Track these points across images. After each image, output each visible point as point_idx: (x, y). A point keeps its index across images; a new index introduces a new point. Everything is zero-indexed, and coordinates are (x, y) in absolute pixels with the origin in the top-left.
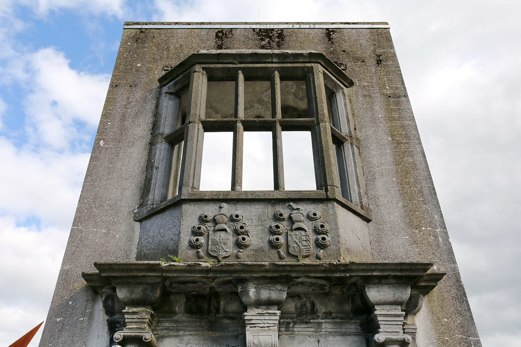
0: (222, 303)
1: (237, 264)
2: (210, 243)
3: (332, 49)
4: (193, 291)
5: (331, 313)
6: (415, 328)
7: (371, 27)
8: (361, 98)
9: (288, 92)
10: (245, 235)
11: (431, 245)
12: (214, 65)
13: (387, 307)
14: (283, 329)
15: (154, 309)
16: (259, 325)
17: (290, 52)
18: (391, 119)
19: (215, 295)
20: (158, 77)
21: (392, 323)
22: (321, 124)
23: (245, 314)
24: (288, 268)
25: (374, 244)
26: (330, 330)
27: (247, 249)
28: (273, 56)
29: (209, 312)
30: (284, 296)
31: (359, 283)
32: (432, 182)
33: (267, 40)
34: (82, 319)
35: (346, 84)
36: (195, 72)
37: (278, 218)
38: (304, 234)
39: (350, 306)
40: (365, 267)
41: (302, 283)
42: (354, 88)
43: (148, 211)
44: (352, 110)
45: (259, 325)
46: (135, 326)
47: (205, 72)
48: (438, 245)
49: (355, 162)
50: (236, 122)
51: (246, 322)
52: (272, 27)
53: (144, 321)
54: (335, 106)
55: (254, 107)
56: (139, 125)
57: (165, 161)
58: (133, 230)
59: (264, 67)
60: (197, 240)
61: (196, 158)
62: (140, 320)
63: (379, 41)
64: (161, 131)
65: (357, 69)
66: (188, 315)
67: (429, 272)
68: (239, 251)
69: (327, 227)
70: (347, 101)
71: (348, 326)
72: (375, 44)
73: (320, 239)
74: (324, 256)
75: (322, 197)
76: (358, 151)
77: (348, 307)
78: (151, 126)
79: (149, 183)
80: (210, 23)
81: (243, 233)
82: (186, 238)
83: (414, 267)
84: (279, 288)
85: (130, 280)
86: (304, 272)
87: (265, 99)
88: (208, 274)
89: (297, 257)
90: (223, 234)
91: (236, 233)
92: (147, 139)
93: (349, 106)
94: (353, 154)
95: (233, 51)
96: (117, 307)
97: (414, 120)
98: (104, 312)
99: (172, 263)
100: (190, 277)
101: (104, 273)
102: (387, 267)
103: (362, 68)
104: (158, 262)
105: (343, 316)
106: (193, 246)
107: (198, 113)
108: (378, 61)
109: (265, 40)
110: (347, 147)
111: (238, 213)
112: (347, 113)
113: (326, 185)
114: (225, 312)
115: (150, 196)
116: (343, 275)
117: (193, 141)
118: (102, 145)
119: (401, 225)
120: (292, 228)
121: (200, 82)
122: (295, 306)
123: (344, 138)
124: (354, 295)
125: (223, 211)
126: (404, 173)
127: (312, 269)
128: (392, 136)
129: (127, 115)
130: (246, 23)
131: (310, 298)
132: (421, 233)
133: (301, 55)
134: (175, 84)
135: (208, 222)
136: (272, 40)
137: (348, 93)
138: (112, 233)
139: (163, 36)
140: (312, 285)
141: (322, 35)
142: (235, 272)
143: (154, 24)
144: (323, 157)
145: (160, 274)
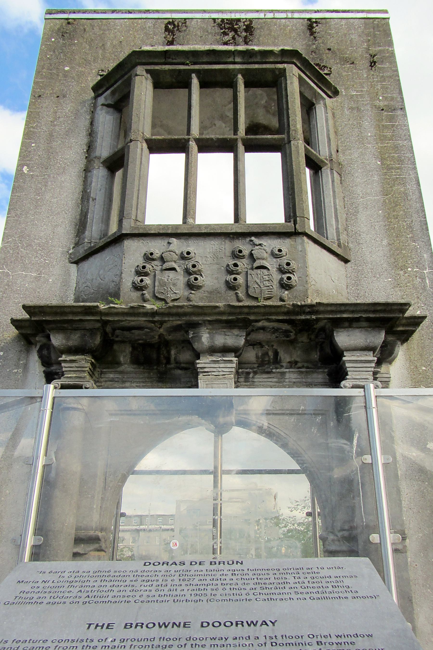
0: (173, 352)
1: (187, 306)
2: (157, 284)
3: (314, 46)
4: (139, 340)
5: (296, 362)
6: (388, 376)
7: (365, 17)
8: (347, 112)
9: (257, 104)
10: (198, 274)
11: (416, 289)
12: (160, 66)
13: (358, 353)
14: (242, 380)
15: (94, 357)
16: (213, 373)
17: (256, 48)
18: (382, 138)
19: (164, 344)
20: (91, 85)
21: (361, 369)
22: (292, 142)
23: (197, 361)
24: (246, 310)
25: (351, 287)
26: (294, 380)
27: (200, 291)
28: (236, 53)
29: (158, 363)
30: (242, 342)
31: (327, 326)
32: (425, 215)
33: (231, 34)
34: (16, 371)
35: (329, 93)
36: (137, 75)
37: (237, 255)
38: (267, 273)
39: (318, 353)
40: (333, 308)
41: (263, 328)
42: (338, 99)
43: (85, 250)
44: (335, 126)
45: (213, 373)
46: (75, 375)
47: (149, 75)
48: (424, 288)
49: (334, 192)
50: (188, 140)
51: (199, 370)
52: (238, 16)
53: (84, 369)
54: (314, 122)
55: (215, 125)
56: (71, 147)
57: (103, 191)
58: (68, 273)
59: (224, 70)
60: (142, 281)
61: (139, 185)
62: (79, 369)
63: (375, 35)
64: (97, 153)
65: (344, 74)
66: (135, 366)
67: (407, 314)
68: (191, 293)
69: (293, 265)
70: (330, 115)
71: (315, 375)
72: (369, 40)
73: (285, 278)
74: (289, 298)
75: (291, 230)
76: (339, 178)
77: (315, 356)
78: (85, 148)
79: (85, 218)
80: (158, 11)
81: (195, 273)
82: (129, 278)
83: (389, 308)
84: (236, 333)
85: (66, 325)
86: (264, 314)
87: (228, 115)
88: (154, 317)
89: (257, 298)
90: (171, 274)
91: (188, 272)
92: (82, 164)
93: (331, 122)
94: (333, 181)
95: (186, 48)
96: (53, 356)
97: (410, 140)
98: (41, 364)
99: (112, 305)
100: (134, 321)
101: (34, 316)
102: (358, 308)
103: (351, 72)
104: (95, 304)
105: (310, 366)
106: (137, 288)
107: (141, 129)
108: (371, 63)
109: (228, 34)
110: (326, 172)
111: (190, 249)
112: (328, 130)
113: (295, 216)
114: (177, 363)
115: (87, 233)
116: (308, 317)
117: (135, 164)
118: (26, 172)
119: (385, 265)
120: (253, 267)
121: (143, 89)
122: (256, 354)
123: (323, 161)
124: (323, 342)
125: (172, 247)
126: (393, 205)
127: (273, 310)
128: (382, 160)
129: (54, 134)
130: (205, 11)
131: (273, 346)
132: (406, 275)
133: (271, 52)
134: (113, 93)
135: (153, 260)
136: (238, 35)
137: (331, 105)
138: (44, 277)
139: (96, 30)
140: (275, 330)
141: (302, 27)
142: (185, 314)
143: (85, 12)
144: (293, 183)
145: (98, 318)
